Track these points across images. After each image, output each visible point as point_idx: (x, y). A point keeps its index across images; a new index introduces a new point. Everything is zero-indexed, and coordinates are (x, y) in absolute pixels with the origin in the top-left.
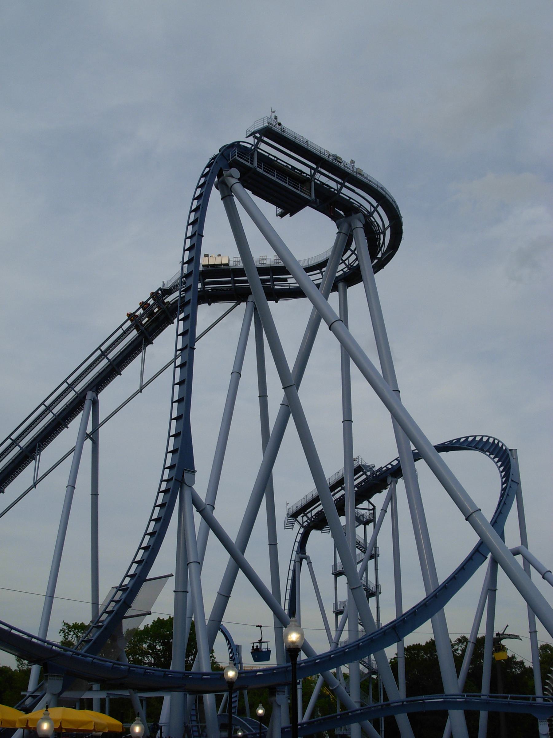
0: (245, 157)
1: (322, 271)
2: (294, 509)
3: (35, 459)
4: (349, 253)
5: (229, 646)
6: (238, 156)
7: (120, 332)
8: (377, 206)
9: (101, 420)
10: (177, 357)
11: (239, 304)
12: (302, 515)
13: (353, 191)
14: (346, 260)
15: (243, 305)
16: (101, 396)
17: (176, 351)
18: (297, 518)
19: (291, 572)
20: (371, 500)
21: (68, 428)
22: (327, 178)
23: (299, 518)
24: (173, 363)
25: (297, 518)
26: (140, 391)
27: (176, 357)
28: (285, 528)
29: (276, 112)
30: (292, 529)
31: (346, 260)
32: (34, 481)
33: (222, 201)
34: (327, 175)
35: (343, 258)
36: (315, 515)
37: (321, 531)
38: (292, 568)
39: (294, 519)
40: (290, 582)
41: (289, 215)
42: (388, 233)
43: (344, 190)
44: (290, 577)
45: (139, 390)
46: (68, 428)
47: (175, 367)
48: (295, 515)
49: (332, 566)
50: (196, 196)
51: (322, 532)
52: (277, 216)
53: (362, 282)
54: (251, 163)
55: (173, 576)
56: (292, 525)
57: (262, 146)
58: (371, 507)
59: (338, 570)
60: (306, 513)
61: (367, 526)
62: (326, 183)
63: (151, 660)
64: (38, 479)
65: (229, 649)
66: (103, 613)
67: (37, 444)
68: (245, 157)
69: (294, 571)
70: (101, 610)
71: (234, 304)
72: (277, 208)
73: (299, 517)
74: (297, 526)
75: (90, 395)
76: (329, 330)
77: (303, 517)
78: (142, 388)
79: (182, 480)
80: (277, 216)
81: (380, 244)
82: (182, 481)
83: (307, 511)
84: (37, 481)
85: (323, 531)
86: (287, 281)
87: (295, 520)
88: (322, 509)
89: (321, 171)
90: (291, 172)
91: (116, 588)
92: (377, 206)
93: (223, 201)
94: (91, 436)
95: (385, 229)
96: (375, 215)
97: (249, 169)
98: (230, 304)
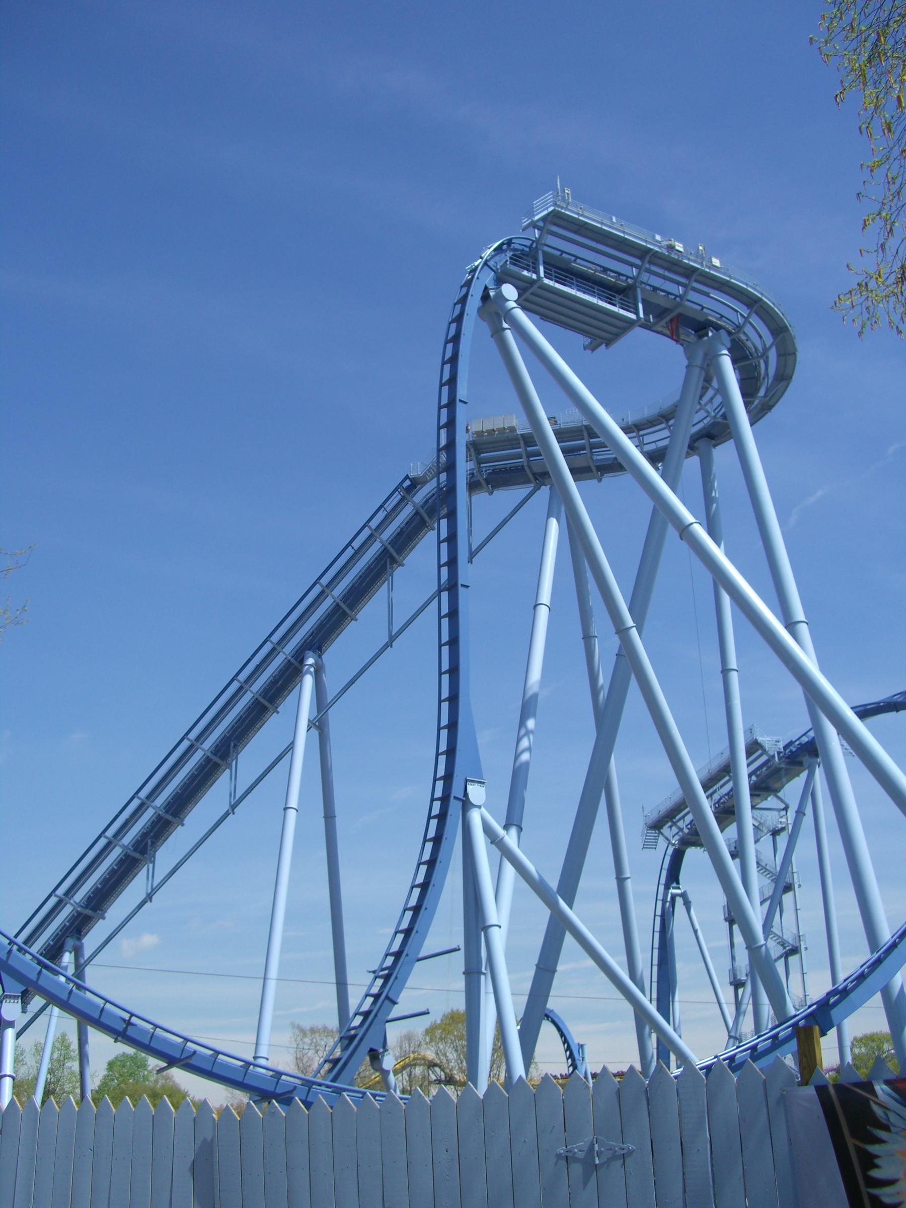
0: (522, 263)
1: (669, 424)
2: (654, 816)
4: (710, 393)
5: (566, 1045)
6: (511, 263)
7: (350, 552)
8: (749, 315)
11: (539, 489)
12: (670, 824)
13: (707, 295)
18: (662, 831)
19: (658, 919)
20: (780, 794)
21: (278, 712)
22: (660, 279)
23: (666, 830)
24: (437, 598)
25: (662, 831)
26: (389, 644)
28: (643, 848)
30: (655, 848)
33: (493, 339)
34: (661, 274)
38: (659, 912)
39: (657, 832)
40: (657, 935)
41: (603, 346)
42: (772, 355)
43: (692, 296)
44: (657, 928)
46: (278, 712)
48: (657, 826)
49: (724, 907)
50: (449, 338)
52: (585, 349)
53: (732, 441)
55: (459, 949)
56: (655, 839)
57: (551, 240)
60: (674, 820)
62: (662, 288)
63: (439, 1074)
65: (566, 1051)
66: (356, 1014)
68: (522, 263)
69: (663, 916)
70: (352, 1012)
73: (664, 828)
74: (662, 843)
76: (680, 539)
77: (671, 827)
78: (392, 640)
79: (464, 796)
80: (585, 349)
81: (760, 375)
82: (464, 799)
83: (677, 818)
88: (692, 820)
89: (649, 269)
90: (602, 277)
91: (374, 972)
94: (317, 724)
95: (766, 350)
96: (748, 329)
97: (532, 282)
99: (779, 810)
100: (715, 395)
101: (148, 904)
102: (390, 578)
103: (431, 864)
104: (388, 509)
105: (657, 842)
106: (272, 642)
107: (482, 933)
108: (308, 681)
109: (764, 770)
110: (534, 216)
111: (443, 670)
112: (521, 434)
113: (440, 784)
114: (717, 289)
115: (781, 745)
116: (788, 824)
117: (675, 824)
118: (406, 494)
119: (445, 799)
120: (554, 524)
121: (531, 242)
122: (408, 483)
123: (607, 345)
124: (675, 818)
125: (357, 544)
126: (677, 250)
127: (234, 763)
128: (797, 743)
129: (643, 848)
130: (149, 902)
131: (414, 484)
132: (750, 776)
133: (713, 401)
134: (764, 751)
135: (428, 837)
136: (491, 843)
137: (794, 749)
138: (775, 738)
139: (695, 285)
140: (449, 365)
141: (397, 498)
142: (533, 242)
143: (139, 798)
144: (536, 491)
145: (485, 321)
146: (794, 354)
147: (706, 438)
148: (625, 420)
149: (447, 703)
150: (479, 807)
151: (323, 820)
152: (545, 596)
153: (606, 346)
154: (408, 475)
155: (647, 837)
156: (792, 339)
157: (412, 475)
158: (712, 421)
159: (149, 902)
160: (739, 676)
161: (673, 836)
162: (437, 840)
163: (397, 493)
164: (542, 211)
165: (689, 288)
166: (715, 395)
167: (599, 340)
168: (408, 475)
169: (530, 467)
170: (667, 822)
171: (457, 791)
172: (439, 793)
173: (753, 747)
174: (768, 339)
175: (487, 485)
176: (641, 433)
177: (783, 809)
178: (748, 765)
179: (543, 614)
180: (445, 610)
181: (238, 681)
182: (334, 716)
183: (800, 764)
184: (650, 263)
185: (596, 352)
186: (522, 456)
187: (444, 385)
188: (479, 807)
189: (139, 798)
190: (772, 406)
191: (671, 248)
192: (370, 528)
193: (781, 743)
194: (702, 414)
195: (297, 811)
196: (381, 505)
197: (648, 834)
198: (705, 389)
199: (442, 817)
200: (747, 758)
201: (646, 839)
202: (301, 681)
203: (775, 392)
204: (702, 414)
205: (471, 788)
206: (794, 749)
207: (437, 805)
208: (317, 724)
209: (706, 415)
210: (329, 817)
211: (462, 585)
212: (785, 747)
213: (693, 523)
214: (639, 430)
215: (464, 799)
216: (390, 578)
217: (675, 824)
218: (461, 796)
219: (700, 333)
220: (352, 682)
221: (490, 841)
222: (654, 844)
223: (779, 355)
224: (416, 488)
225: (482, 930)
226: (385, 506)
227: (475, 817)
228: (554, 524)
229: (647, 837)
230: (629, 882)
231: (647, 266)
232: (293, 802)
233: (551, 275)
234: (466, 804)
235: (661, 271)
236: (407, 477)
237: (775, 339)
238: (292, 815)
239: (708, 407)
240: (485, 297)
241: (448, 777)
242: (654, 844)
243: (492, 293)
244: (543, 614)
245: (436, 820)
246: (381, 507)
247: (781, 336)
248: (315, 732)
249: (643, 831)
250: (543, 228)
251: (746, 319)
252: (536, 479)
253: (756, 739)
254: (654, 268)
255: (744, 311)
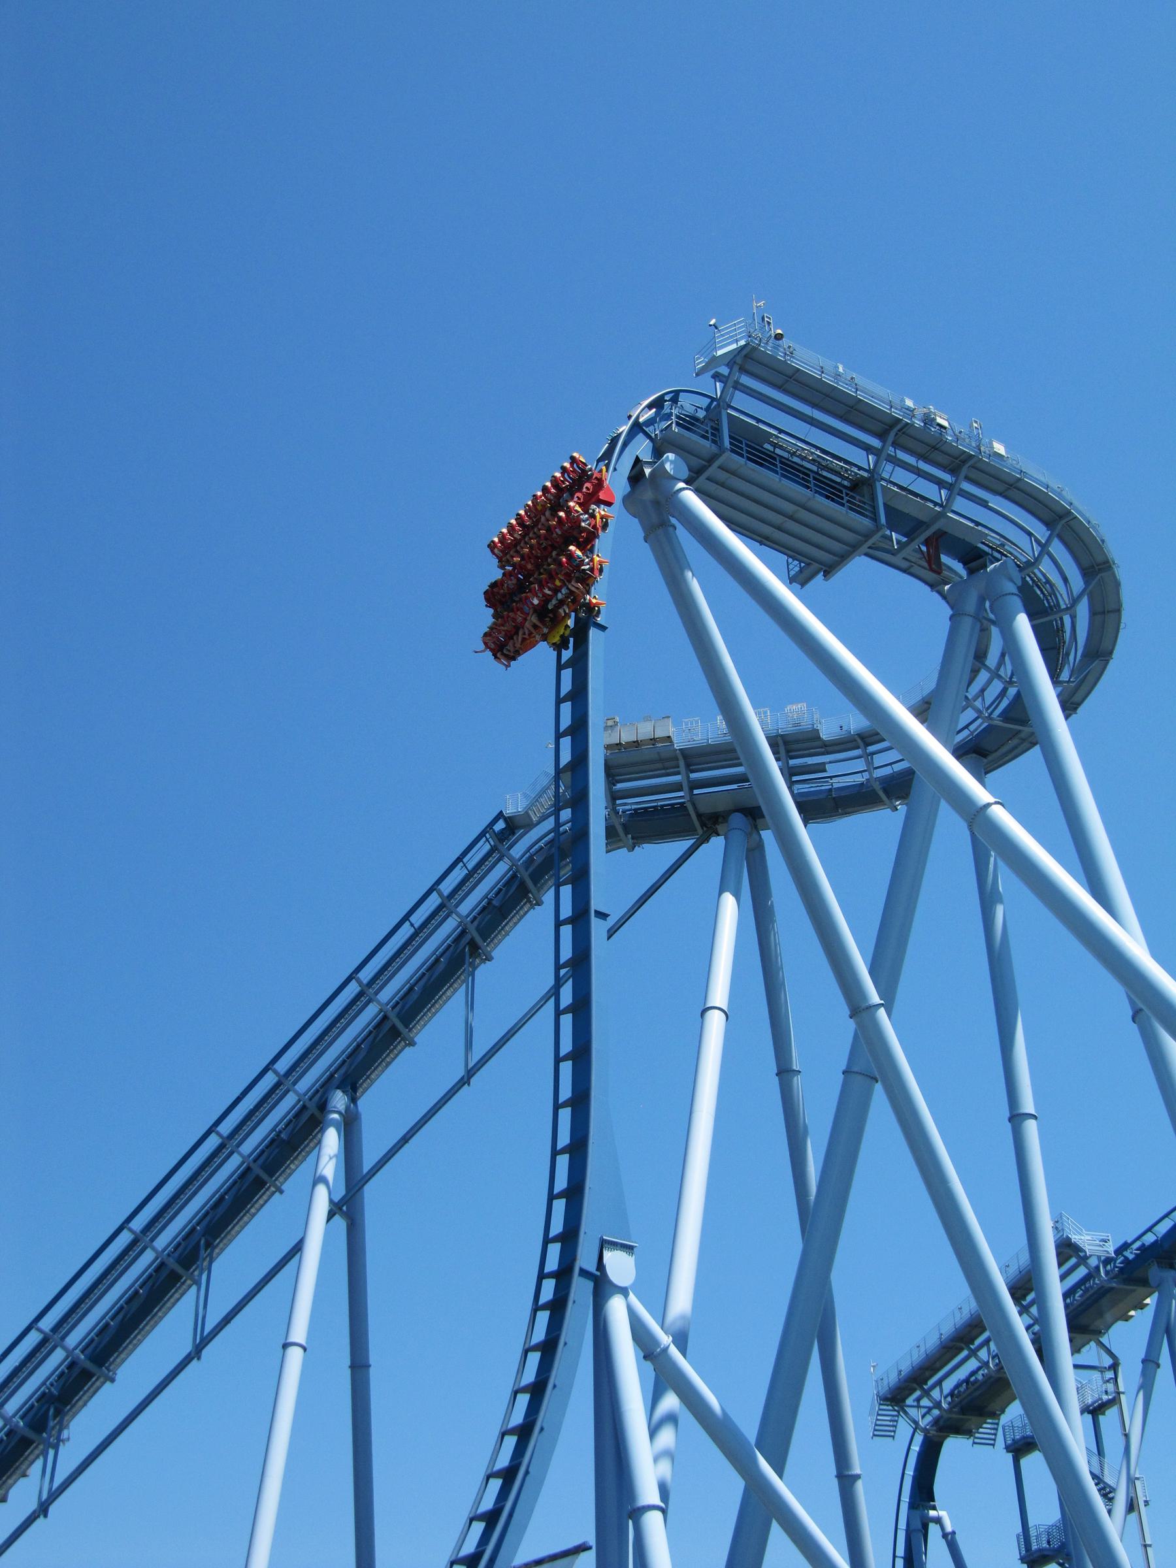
3: (197, 1283)
4: (983, 676)
6: (678, 424)
7: (406, 931)
8: (1049, 540)
9: (368, 1161)
10: (562, 982)
12: (918, 1393)
13: (984, 504)
14: (975, 698)
15: (717, 844)
16: (367, 1103)
17: (558, 967)
20: (1104, 1340)
26: (465, 1081)
27: (558, 983)
28: (874, 1435)
29: (605, 935)
31: (975, 698)
32: (195, 1339)
34: (913, 466)
35: (967, 694)
36: (951, 1394)
37: (971, 1440)
41: (820, 576)
43: (960, 504)
45: (462, 1078)
46: (281, 1192)
47: (558, 1013)
49: (1018, 1536)
51: (974, 1443)
54: (714, 442)
55: (590, 1548)
56: (893, 1426)
57: (740, 400)
58: (1108, 1361)
59: (1034, 1547)
60: (925, 1387)
61: (1101, 1417)
64: (206, 1333)
67: (200, 1240)
71: (692, 841)
72: (790, 560)
74: (904, 1428)
75: (339, 1100)
79: (598, 1270)
81: (1064, 643)
82: (598, 1273)
83: (931, 1382)
84: (202, 1339)
85: (976, 1440)
86: (825, 771)
87: (898, 1412)
92: (1049, 540)
93: (651, 546)
98: (680, 846)
99: (1102, 1370)
100: (989, 682)
101: (40, 1521)
102: (470, 978)
103: (537, 1390)
104: (470, 866)
105: (896, 1426)
106: (276, 1072)
107: (630, 1522)
108: (331, 1140)
109: (1077, 1295)
110: (716, 349)
111: (562, 1053)
112: (680, 749)
113: (555, 1250)
114: (1001, 494)
115: (1111, 1248)
116: (1119, 1393)
117: (927, 1393)
118: (498, 843)
119: (563, 1275)
120: (729, 903)
121: (709, 400)
122: (500, 825)
123: (827, 574)
124: (926, 1383)
125: (418, 918)
126: (939, 425)
127: (204, 1277)
128: (1138, 1244)
129: (874, 1435)
130: (42, 1517)
131: (513, 827)
132: (1066, 1295)
133: (985, 693)
134: (1083, 1260)
135: (559, 1147)
136: (645, 1357)
137: (1131, 1257)
138: (1103, 1235)
139: (966, 486)
140: (569, 703)
141: (484, 848)
142: (713, 399)
143: (39, 1330)
144: (701, 845)
145: (636, 517)
146: (1118, 611)
147: (974, 755)
148: (845, 728)
149: (570, 1063)
150: (624, 1291)
151: (348, 1372)
152: (719, 994)
153: (825, 576)
154: (501, 812)
155: (879, 1418)
156: (1117, 585)
157: (509, 811)
158: (986, 724)
159: (42, 1517)
160: (1038, 1126)
161: (923, 1417)
162: (548, 1348)
163: (484, 839)
164: (729, 344)
165: (956, 490)
166: (989, 682)
167: (815, 566)
168: (501, 812)
169: (694, 805)
170: (913, 1391)
171: (585, 1259)
172: (552, 1265)
173: (1067, 1250)
174: (1077, 582)
175: (626, 836)
176: (871, 749)
177: (1110, 1368)
178: (1063, 1277)
179: (715, 1023)
180: (566, 911)
181: (219, 1134)
182: (371, 1192)
183: (1144, 1282)
184: (895, 444)
185: (808, 586)
186: (681, 786)
187: (564, 700)
188: (624, 1291)
189: (39, 1330)
190: (1079, 704)
191: (928, 420)
192: (440, 894)
193: (1111, 1243)
194: (970, 714)
195: (305, 1349)
196: (458, 858)
197: (880, 1412)
198: (975, 672)
199: (558, 1307)
200: (1060, 1265)
201: (877, 1420)
202: (319, 1142)
203: (1089, 672)
204: (970, 714)
205: (609, 1256)
206: (1131, 1257)
207: (549, 1286)
208: (344, 1208)
209: (976, 715)
210: (359, 1366)
211: (596, 911)
212: (1119, 1251)
213: (992, 804)
214: (867, 745)
215: (598, 1273)
216: (470, 978)
217: (927, 1393)
218: (592, 1267)
219: (973, 565)
220: (405, 1140)
221: (643, 1354)
222: (892, 1429)
223: (1093, 613)
224: (514, 834)
225: (630, 1517)
226: (465, 860)
227: (617, 1308)
228: (729, 903)
229: (879, 1418)
230: (860, 1486)
231: (891, 450)
232: (299, 1333)
233: (741, 449)
234: (602, 1286)
235: (911, 460)
236: (500, 815)
237: (1087, 583)
238: (295, 1357)
239: (978, 704)
240: (636, 477)
241: (569, 1238)
242: (892, 1429)
243: (647, 471)
244: (715, 1023)
245: (567, 1156)
246: (459, 860)
247: (1098, 577)
248: (340, 1222)
249: (872, 1408)
250: (728, 377)
251: (1044, 547)
252: (703, 825)
253: (1068, 1237)
254: (901, 455)
255: (1040, 531)
